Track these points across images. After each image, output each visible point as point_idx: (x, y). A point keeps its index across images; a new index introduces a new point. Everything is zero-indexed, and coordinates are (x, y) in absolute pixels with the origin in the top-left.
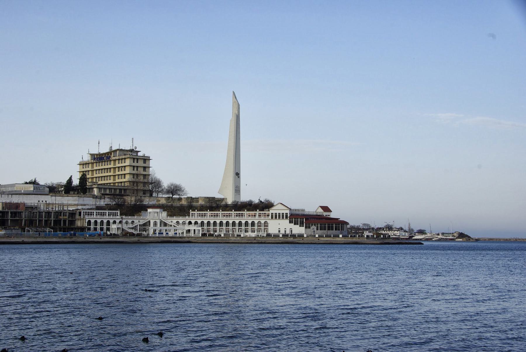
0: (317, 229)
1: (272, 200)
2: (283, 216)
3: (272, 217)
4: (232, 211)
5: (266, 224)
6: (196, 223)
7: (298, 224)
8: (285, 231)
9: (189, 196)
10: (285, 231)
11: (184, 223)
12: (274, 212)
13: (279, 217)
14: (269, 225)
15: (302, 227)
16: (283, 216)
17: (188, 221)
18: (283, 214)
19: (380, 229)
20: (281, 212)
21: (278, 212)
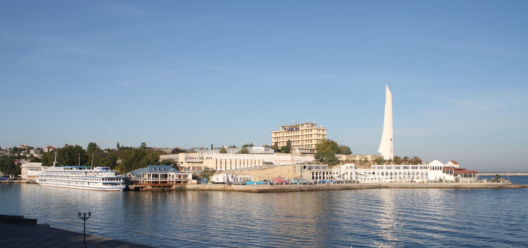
3: (431, 169)
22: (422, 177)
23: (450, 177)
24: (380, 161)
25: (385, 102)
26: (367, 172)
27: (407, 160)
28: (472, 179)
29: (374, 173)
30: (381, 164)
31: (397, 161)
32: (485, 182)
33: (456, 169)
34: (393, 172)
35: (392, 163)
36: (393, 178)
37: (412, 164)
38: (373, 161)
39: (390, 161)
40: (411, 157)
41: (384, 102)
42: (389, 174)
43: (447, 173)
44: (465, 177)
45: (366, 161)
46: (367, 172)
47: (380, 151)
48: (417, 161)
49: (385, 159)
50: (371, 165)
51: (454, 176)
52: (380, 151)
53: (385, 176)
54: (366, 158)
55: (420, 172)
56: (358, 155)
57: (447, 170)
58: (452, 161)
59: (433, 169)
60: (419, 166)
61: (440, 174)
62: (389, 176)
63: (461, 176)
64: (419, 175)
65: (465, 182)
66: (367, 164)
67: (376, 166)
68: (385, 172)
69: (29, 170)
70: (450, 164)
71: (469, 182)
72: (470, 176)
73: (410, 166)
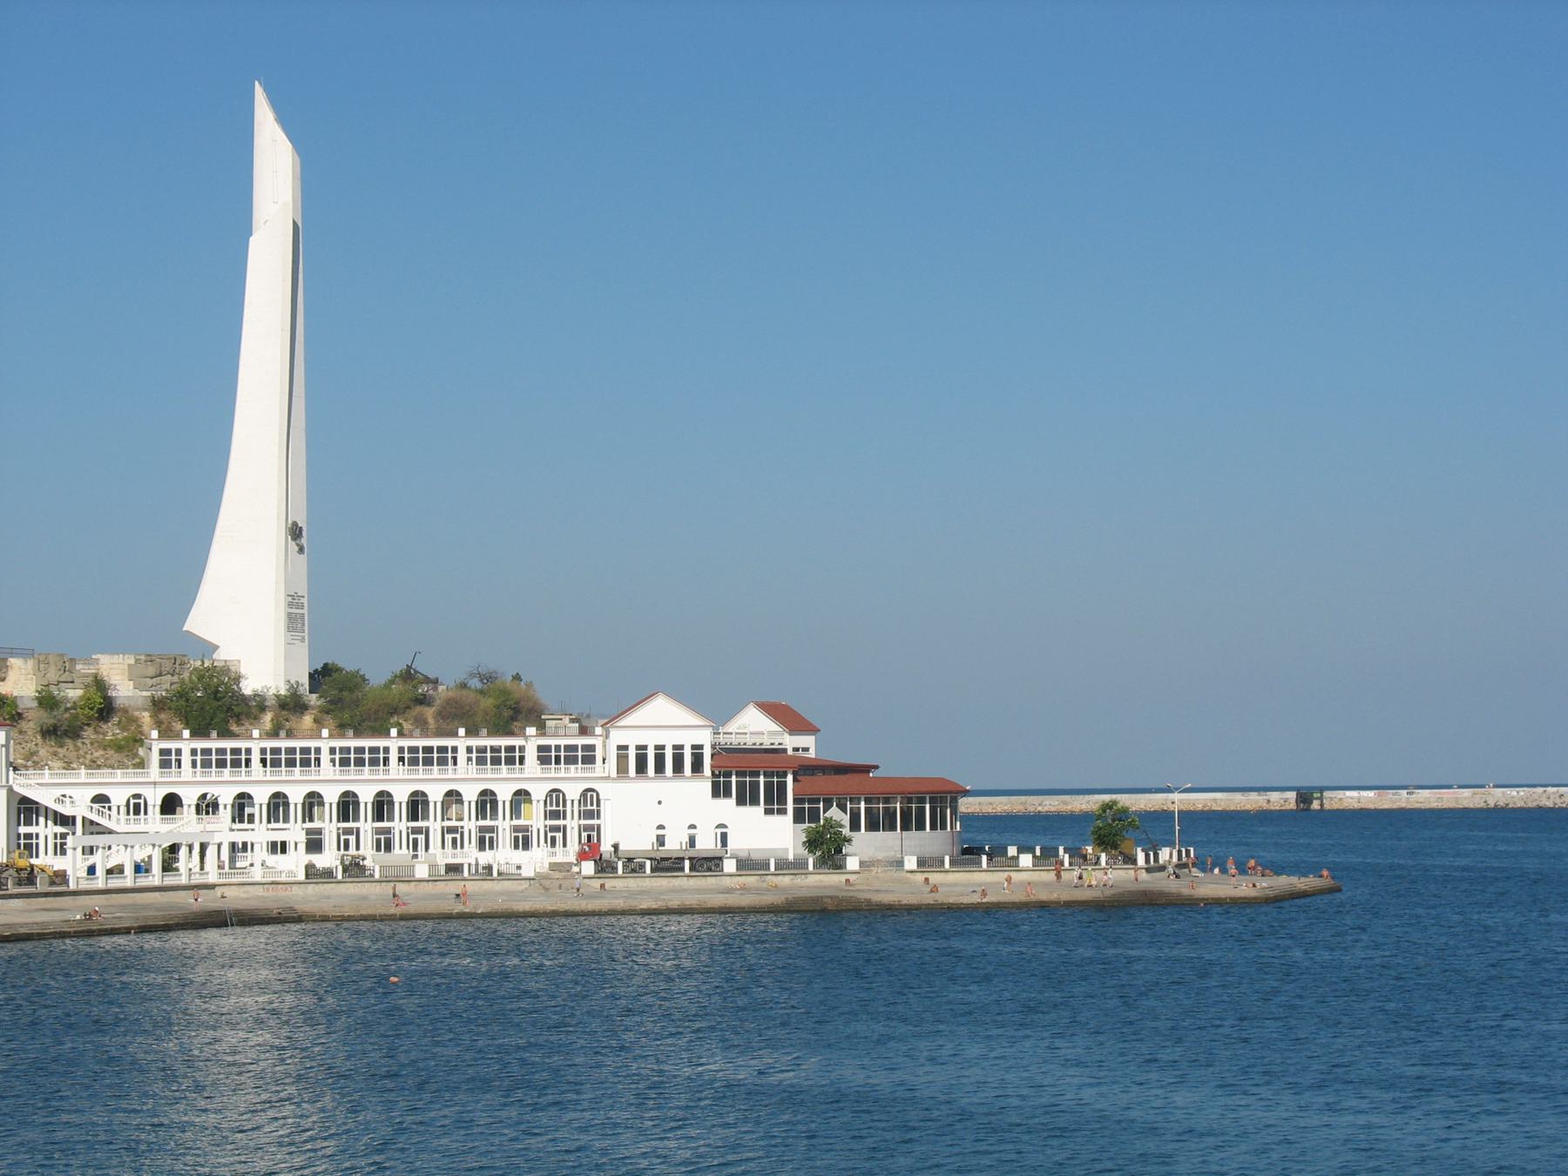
0: (855, 826)
1: (544, 694)
2: (660, 760)
3: (622, 768)
4: (455, 735)
5: (590, 804)
6: (207, 806)
7: (754, 801)
8: (661, 840)
9: (305, 681)
10: (661, 840)
11: (136, 807)
12: (632, 739)
13: (660, 768)
14: (606, 808)
15: (776, 819)
16: (660, 760)
17: (162, 792)
18: (678, 748)
19: (661, 893)
20: (669, 740)
21: (651, 740)
22: (555, 835)
23: (771, 833)
24: (210, 704)
25: (248, 231)
26: (119, 797)
27: (423, 701)
28: (928, 840)
29: (171, 805)
30: (225, 734)
31: (341, 697)
32: (1023, 875)
33: (806, 770)
34: (401, 795)
35: (308, 720)
36: (330, 840)
37: (472, 732)
38: (158, 705)
39: (291, 705)
40: (449, 672)
41: (244, 228)
42: (295, 810)
43: (746, 797)
44: (873, 826)
45: (104, 708)
46: (119, 797)
47: (199, 622)
48: (505, 710)
49: (248, 688)
50: (138, 740)
51: (798, 817)
52: (199, 622)
53: (260, 833)
54: (100, 685)
55: (539, 792)
56: (25, 654)
57: (742, 775)
58: (775, 711)
59: (641, 767)
60: (530, 740)
61: (688, 811)
62: (295, 832)
63: (845, 819)
64: (534, 816)
65: (888, 864)
66: (112, 730)
67: (186, 744)
68: (261, 796)
69: (1030, 865)
70: (753, 727)
71: (911, 863)
72: (912, 821)
73: (462, 742)
